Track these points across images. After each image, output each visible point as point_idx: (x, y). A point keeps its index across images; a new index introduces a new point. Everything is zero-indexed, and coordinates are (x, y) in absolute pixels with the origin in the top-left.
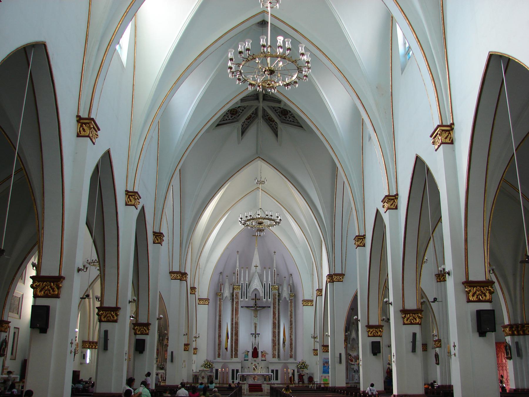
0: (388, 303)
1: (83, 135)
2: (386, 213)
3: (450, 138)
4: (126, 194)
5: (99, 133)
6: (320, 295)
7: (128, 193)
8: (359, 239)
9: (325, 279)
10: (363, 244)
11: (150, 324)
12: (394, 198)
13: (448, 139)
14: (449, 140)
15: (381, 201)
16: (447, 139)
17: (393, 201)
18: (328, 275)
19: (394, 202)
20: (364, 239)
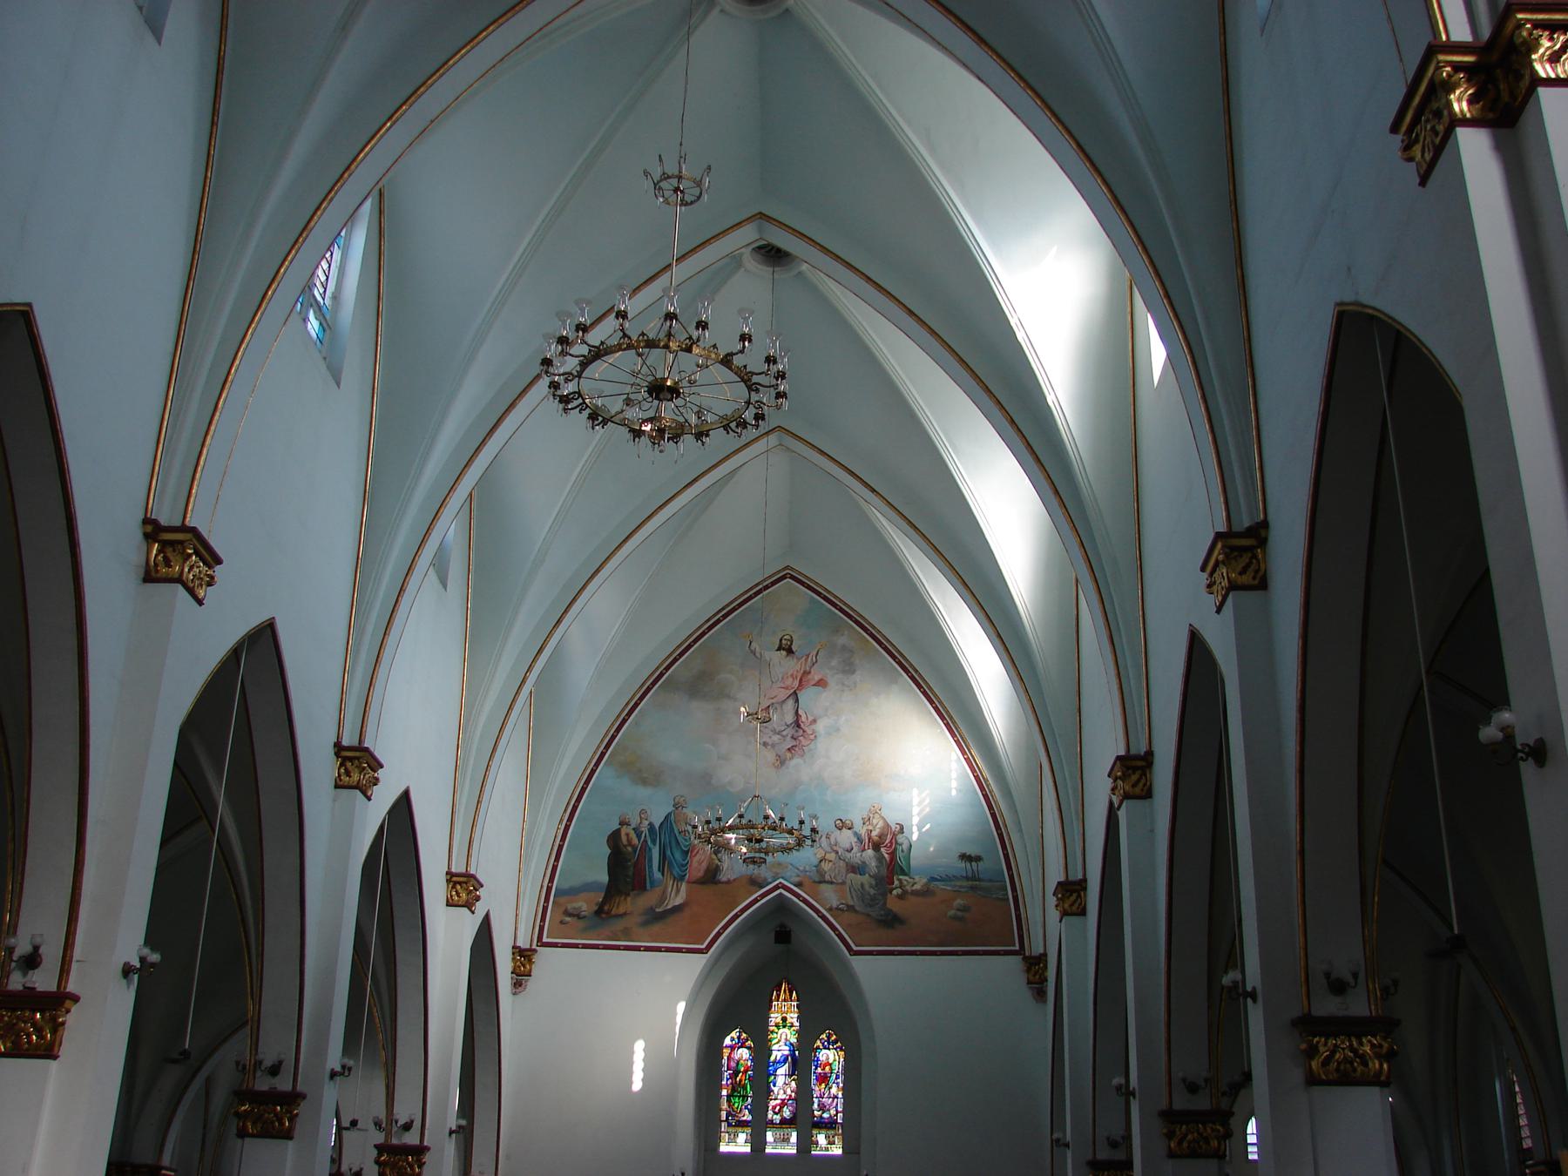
0: (1239, 993)
1: (346, 784)
2: (1430, 183)
3: (1257, 571)
4: (448, 881)
5: (381, 773)
6: (1074, 908)
7: (451, 878)
8: (1130, 771)
9: (1100, 789)
10: (1146, 788)
11: (303, 1096)
12: (1143, 763)
13: (1250, 573)
14: (1254, 578)
15: (1106, 775)
16: (1248, 573)
17: (1250, 555)
18: (1118, 758)
19: (1254, 561)
20: (1082, 893)
